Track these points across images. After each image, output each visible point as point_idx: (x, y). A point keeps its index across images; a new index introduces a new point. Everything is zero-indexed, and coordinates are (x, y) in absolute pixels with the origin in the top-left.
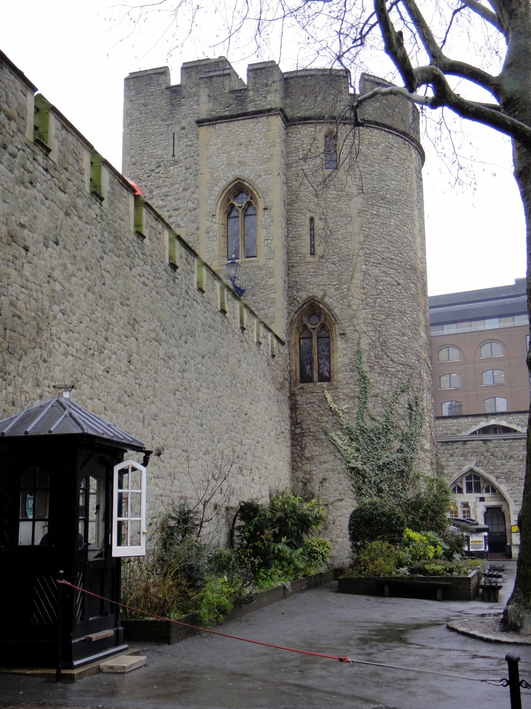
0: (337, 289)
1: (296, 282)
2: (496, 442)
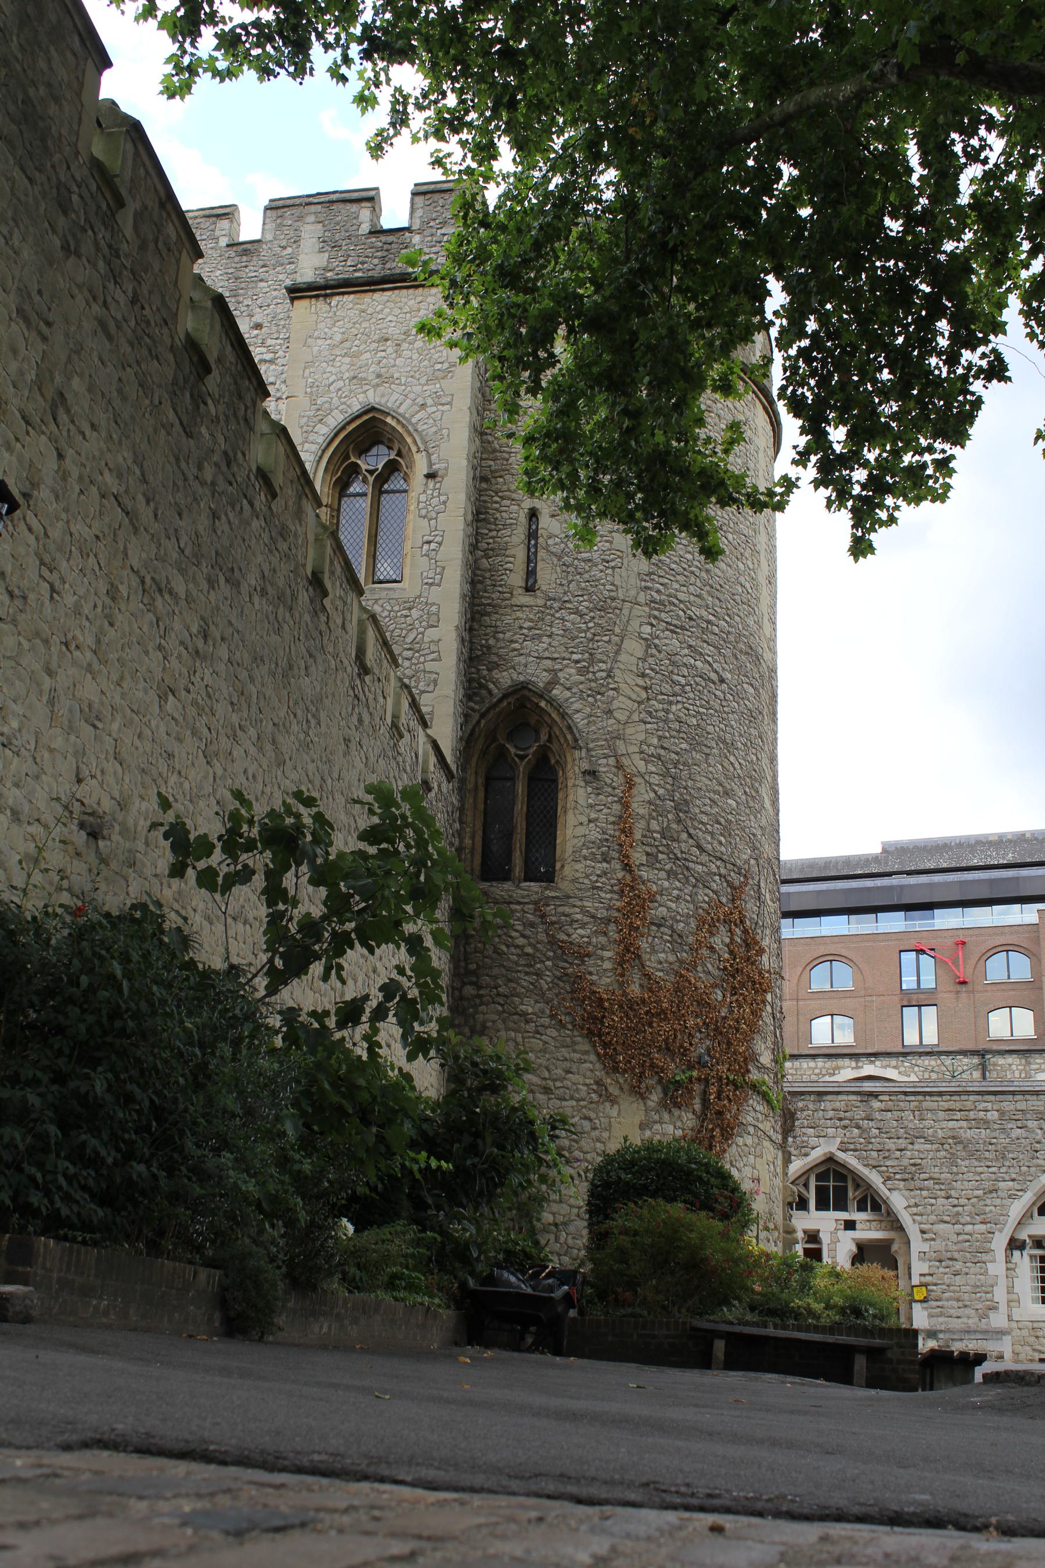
0: (582, 672)
1: (489, 647)
2: (887, 1098)
